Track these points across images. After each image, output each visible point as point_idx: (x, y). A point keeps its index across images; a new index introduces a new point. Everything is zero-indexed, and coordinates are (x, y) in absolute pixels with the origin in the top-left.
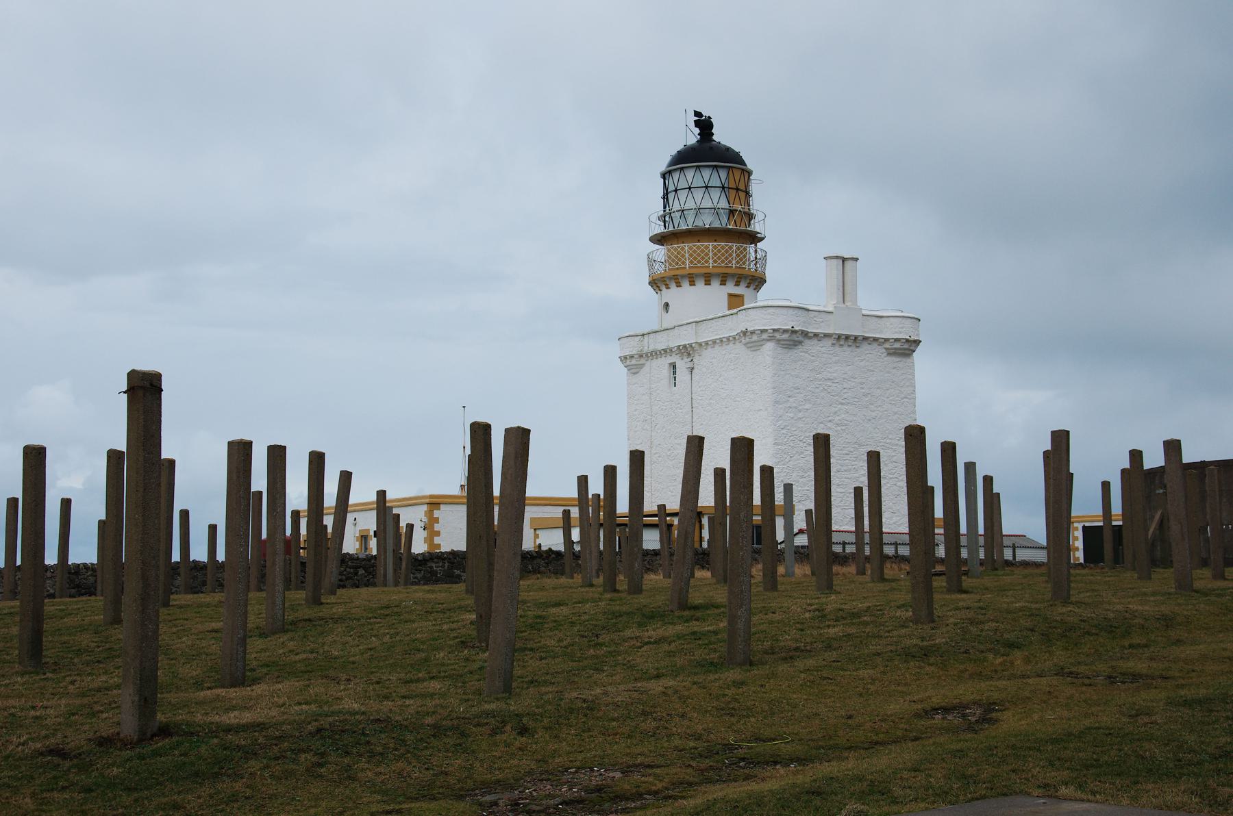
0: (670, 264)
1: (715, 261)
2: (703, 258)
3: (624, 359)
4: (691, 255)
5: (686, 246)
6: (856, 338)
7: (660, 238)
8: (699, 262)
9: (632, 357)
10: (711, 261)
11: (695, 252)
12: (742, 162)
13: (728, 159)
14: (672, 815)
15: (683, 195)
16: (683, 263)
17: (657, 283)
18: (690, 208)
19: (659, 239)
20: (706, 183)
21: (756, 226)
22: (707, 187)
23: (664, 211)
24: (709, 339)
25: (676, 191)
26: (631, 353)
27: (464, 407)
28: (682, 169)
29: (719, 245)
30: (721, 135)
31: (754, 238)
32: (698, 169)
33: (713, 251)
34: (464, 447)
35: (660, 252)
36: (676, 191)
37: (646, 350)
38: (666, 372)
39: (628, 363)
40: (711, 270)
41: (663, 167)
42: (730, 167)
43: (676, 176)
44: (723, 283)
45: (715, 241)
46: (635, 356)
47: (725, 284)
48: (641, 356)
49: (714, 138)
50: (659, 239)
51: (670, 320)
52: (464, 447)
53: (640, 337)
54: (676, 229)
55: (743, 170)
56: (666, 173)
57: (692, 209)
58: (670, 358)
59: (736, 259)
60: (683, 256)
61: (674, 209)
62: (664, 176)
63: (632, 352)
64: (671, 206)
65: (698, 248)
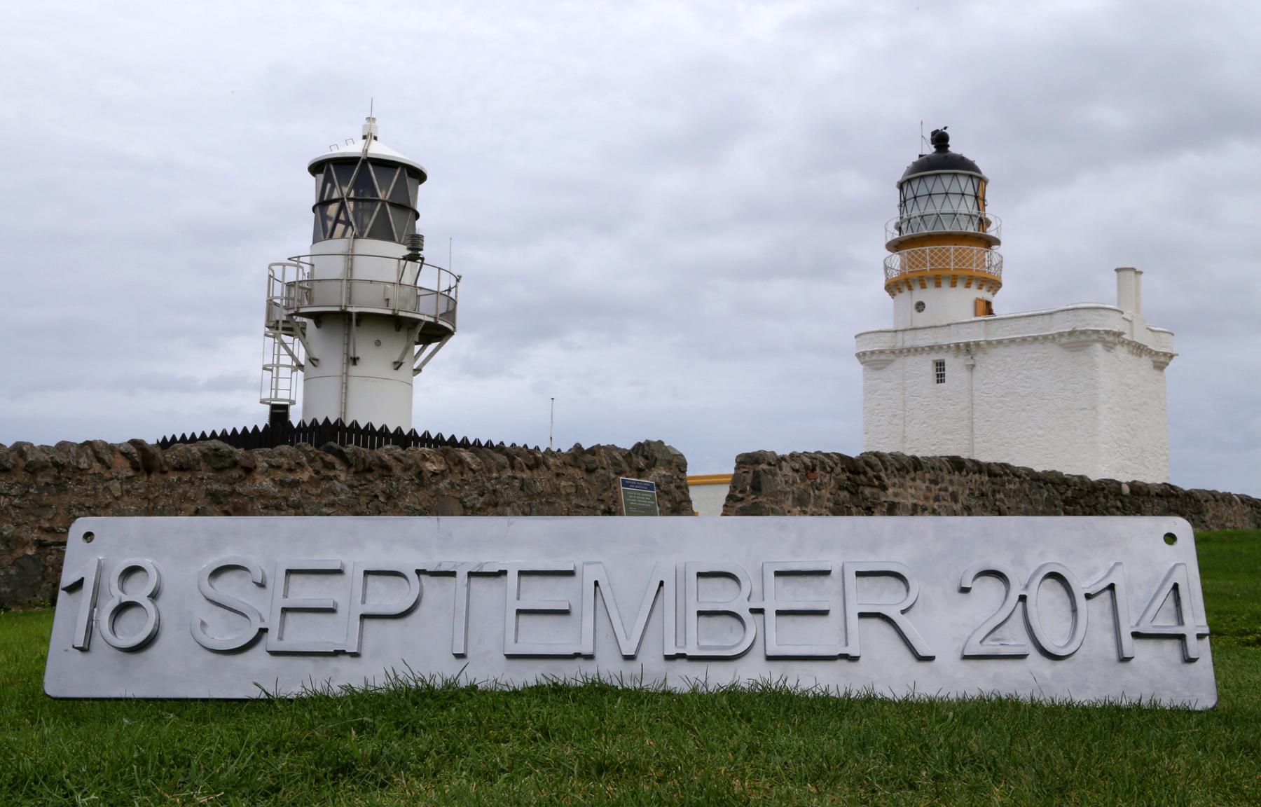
0: (910, 267)
1: (956, 264)
2: (944, 261)
3: (858, 355)
4: (932, 258)
5: (927, 249)
6: (967, 345)
7: (897, 243)
8: (940, 264)
9: (882, 352)
10: (952, 263)
11: (936, 254)
12: (975, 169)
13: (962, 166)
14: (593, 806)
15: (922, 202)
16: (924, 265)
17: (893, 287)
18: (932, 213)
19: (895, 246)
20: (963, 189)
21: (991, 231)
22: (930, 195)
23: (901, 218)
24: (1054, 332)
25: (915, 197)
26: (881, 348)
27: (553, 399)
28: (955, 174)
29: (960, 248)
30: (956, 147)
31: (990, 242)
32: (922, 180)
33: (926, 255)
34: (551, 438)
35: (896, 260)
36: (915, 197)
37: (899, 345)
38: (930, 370)
39: (867, 359)
40: (974, 273)
41: (899, 177)
42: (955, 174)
43: (915, 184)
44: (968, 285)
45: (955, 245)
46: (886, 352)
47: (955, 286)
48: (893, 352)
49: (949, 149)
50: (895, 246)
51: (921, 319)
52: (551, 438)
53: (891, 334)
54: (915, 233)
55: (971, 176)
56: (905, 182)
57: (933, 214)
58: (936, 355)
59: (954, 261)
60: (924, 259)
61: (913, 216)
62: (901, 186)
63: (883, 347)
64: (909, 211)
65: (940, 251)
